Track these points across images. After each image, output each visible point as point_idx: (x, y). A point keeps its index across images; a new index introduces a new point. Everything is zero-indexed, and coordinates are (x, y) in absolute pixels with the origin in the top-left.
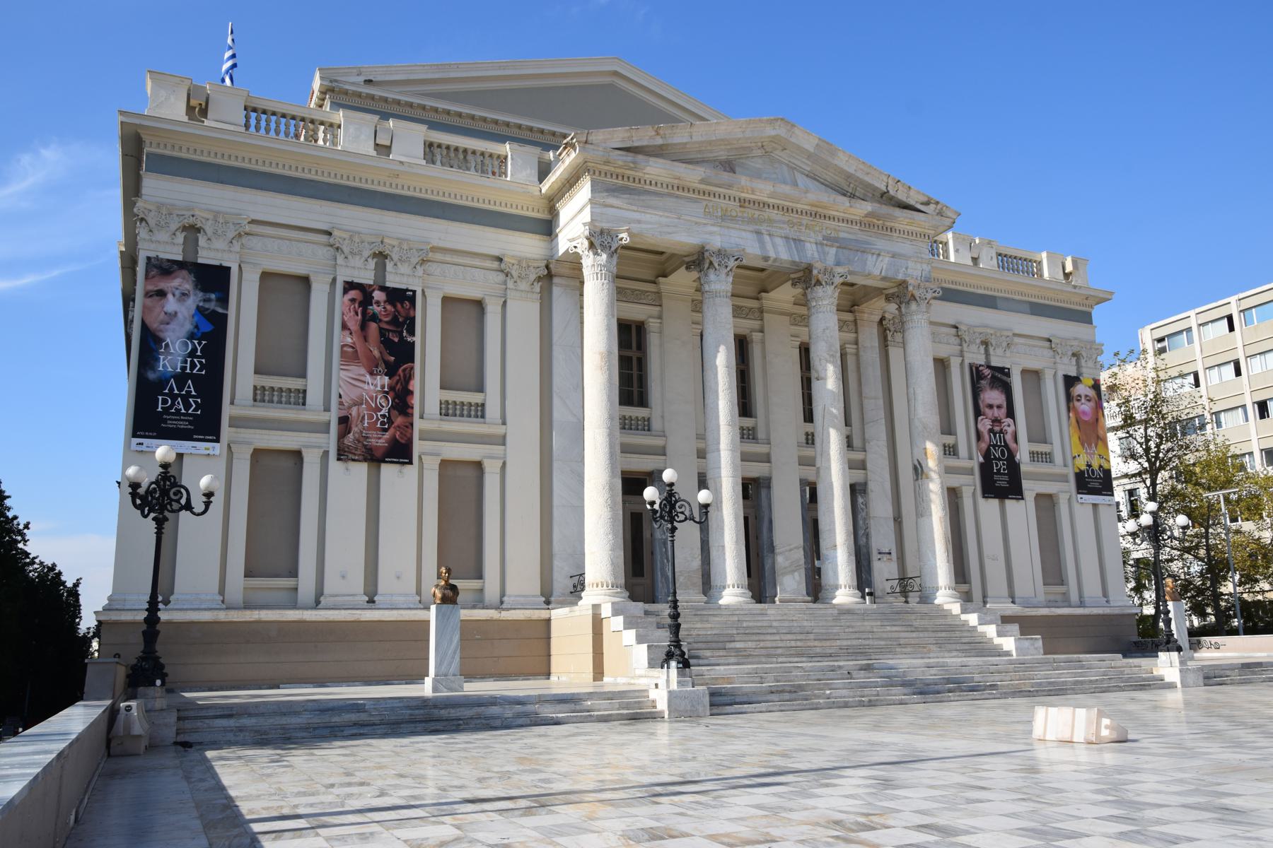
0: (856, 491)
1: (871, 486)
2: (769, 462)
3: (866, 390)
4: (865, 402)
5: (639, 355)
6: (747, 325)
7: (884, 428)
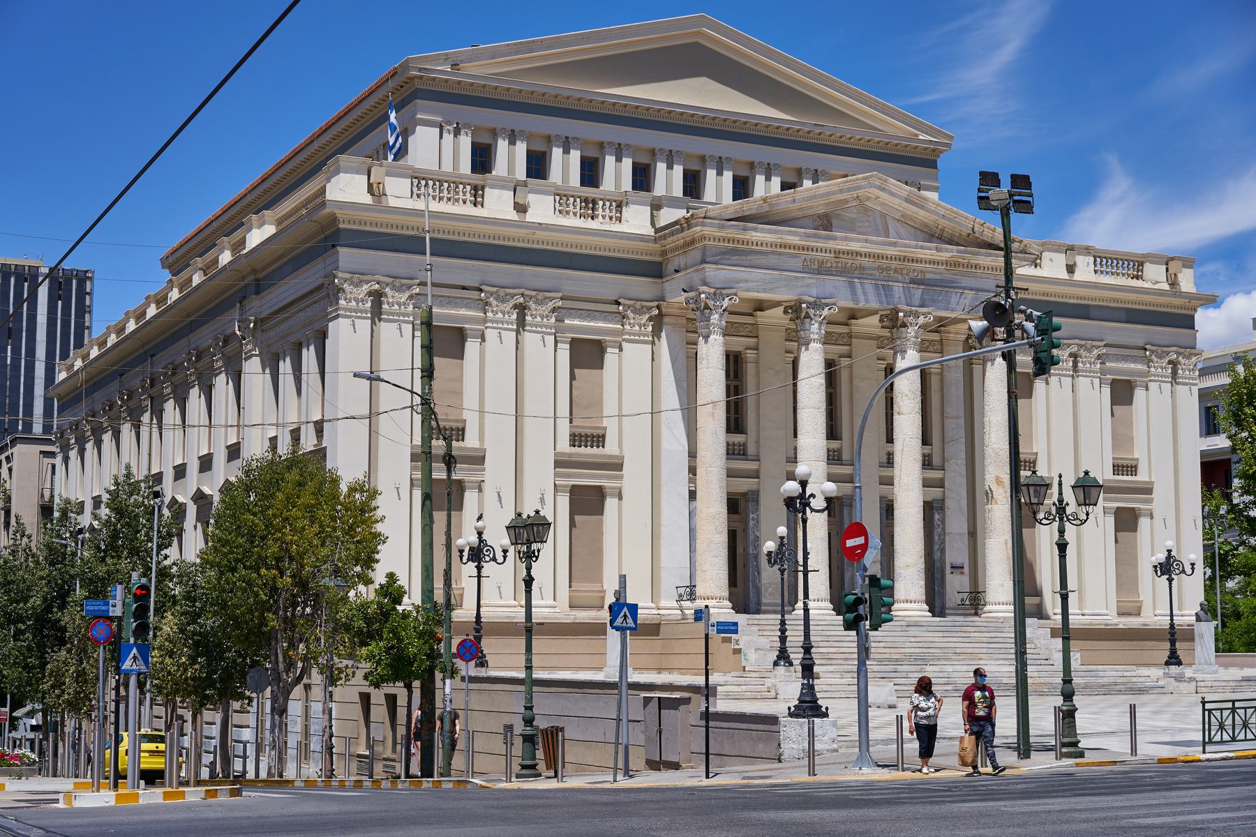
0: (932, 511)
1: (948, 503)
2: (943, 487)
3: (948, 410)
4: (947, 421)
5: (736, 383)
6: (739, 343)
7: (963, 447)
